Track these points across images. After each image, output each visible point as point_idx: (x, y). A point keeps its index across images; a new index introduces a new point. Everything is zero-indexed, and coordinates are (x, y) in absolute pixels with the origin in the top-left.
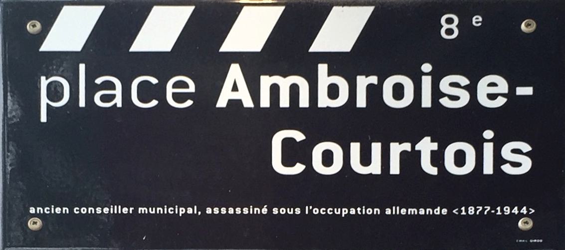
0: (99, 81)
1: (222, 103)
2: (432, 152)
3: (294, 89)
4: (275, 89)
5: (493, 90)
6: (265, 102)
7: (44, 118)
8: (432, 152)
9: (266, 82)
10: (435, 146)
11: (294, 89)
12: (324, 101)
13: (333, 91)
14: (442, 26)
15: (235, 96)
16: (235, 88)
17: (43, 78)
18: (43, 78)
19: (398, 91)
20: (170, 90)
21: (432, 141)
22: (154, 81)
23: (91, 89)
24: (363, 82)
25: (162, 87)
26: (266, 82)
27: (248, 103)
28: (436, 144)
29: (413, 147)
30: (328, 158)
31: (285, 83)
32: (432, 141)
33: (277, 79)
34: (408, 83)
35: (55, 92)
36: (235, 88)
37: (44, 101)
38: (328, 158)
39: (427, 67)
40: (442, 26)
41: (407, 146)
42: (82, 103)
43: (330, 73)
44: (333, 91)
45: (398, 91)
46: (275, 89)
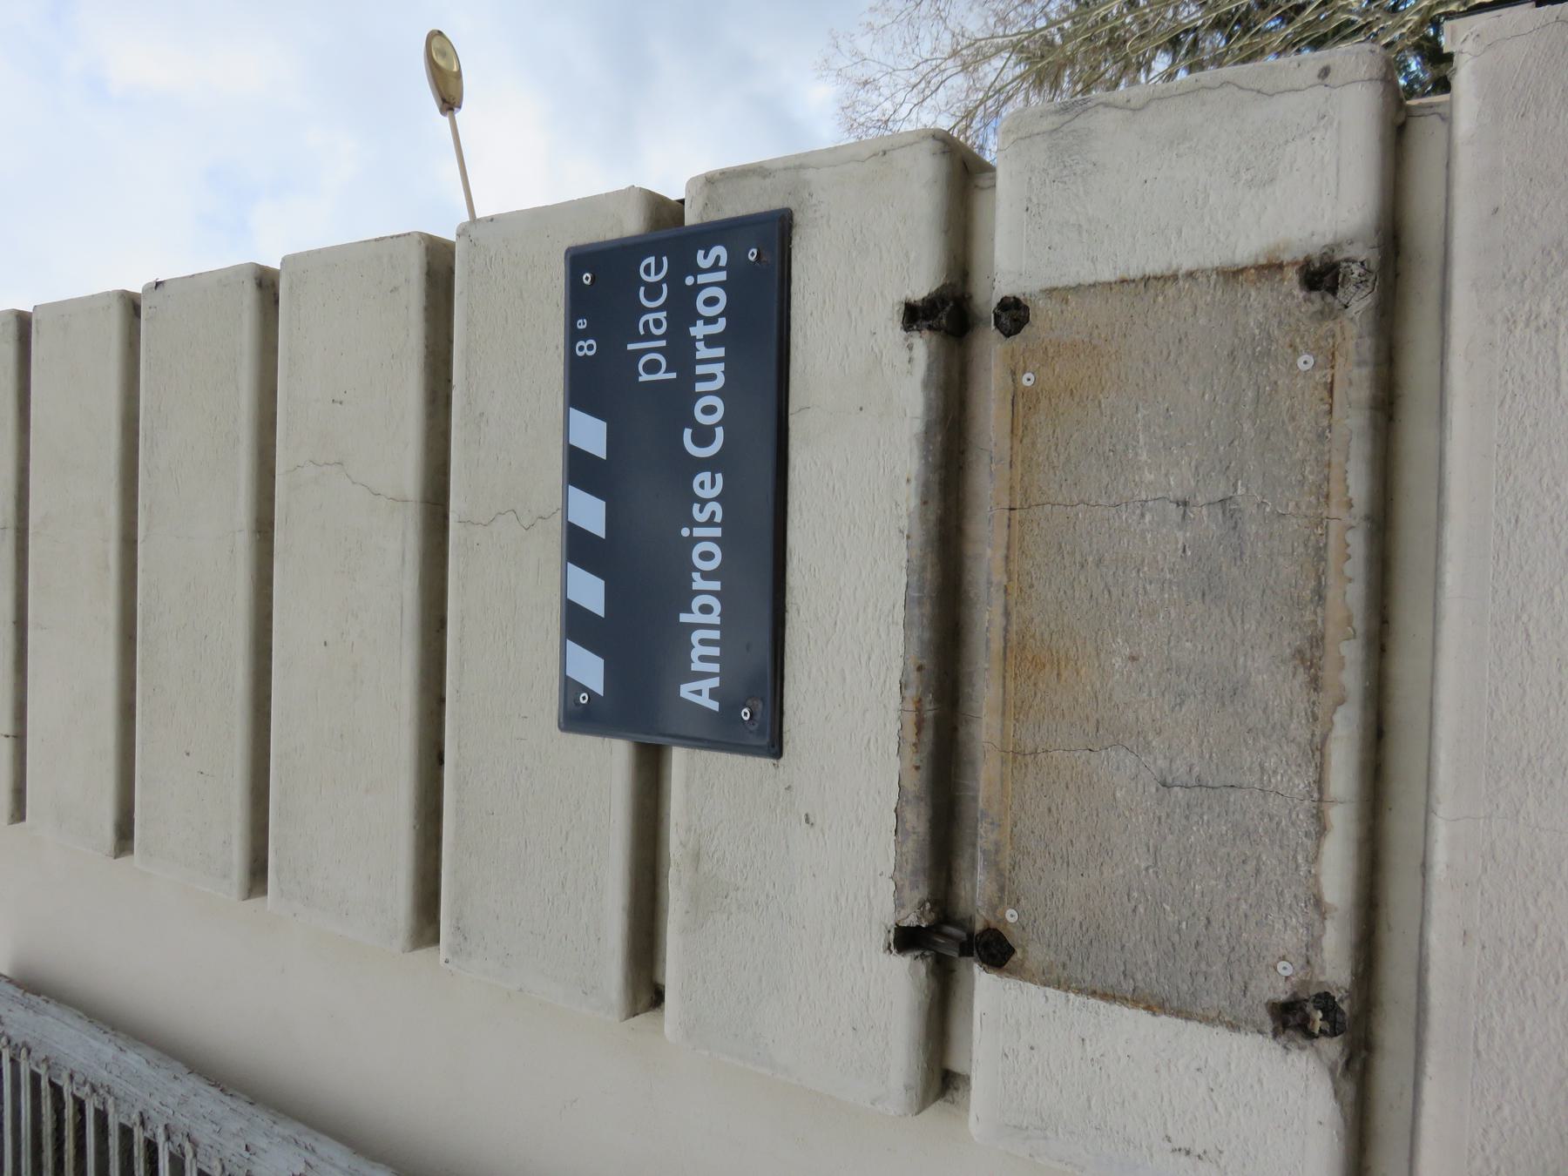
0: (642, 332)
1: (714, 706)
2: (705, 324)
3: (703, 642)
4: (703, 659)
5: (708, 484)
6: (715, 668)
7: (673, 375)
8: (705, 324)
9: (697, 666)
10: (700, 323)
11: (703, 642)
12: (714, 618)
13: (706, 609)
14: (585, 354)
15: (706, 693)
16: (699, 693)
17: (641, 379)
18: (641, 379)
19: (707, 556)
20: (653, 278)
21: (695, 325)
22: (642, 289)
23: (649, 336)
24: (698, 583)
25: (647, 284)
26: (697, 666)
27: (715, 682)
28: (698, 322)
29: (700, 340)
30: (709, 410)
31: (698, 651)
32: (695, 325)
33: (695, 654)
34: (700, 548)
35: (652, 367)
36: (699, 693)
37: (661, 376)
38: (709, 410)
39: (685, 532)
40: (585, 354)
41: (700, 345)
42: (663, 343)
43: (690, 611)
44: (706, 609)
45: (707, 556)
46: (703, 659)
